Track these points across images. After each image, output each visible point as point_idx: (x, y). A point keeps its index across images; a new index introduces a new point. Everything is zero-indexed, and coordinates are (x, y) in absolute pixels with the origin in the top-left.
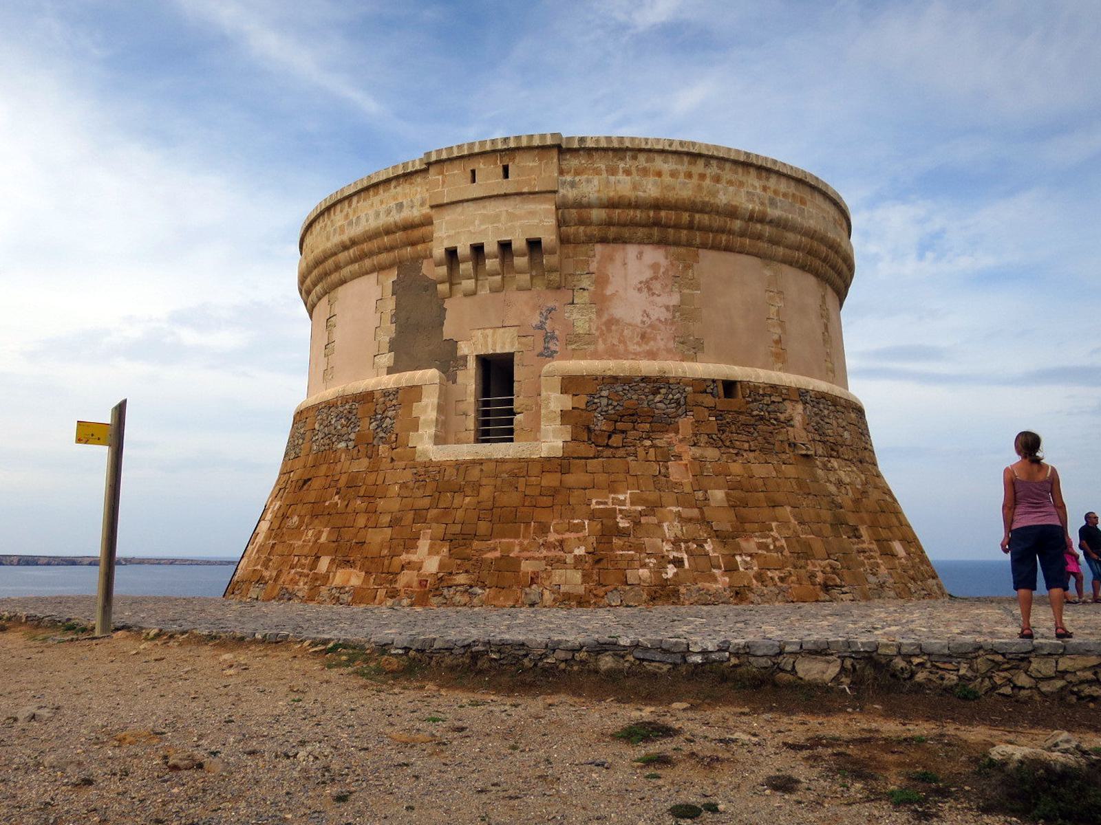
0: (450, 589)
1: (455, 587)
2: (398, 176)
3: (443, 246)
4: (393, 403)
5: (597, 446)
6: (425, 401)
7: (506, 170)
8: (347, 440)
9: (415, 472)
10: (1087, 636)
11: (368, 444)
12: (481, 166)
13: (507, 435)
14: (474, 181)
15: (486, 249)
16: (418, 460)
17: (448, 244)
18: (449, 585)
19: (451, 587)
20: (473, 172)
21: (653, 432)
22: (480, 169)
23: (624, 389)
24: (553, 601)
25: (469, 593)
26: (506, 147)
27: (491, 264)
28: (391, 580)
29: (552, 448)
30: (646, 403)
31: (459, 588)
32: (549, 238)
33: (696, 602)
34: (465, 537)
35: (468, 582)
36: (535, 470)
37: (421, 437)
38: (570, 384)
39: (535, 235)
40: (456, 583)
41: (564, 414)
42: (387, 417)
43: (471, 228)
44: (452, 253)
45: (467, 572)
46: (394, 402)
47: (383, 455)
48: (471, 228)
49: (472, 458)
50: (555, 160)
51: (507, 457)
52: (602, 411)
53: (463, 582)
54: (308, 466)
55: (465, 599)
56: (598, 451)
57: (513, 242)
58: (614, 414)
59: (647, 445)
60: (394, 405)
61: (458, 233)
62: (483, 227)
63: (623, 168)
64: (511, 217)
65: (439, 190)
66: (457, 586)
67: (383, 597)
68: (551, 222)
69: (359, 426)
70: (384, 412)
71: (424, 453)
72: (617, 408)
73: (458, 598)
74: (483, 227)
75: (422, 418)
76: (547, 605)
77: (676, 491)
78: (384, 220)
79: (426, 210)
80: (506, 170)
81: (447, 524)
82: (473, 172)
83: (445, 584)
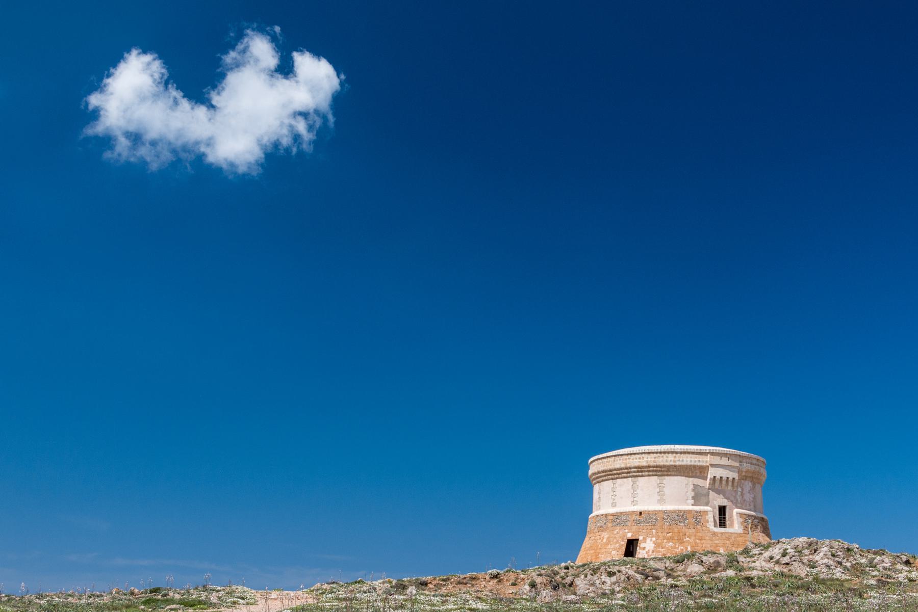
6: (709, 516)
71: (712, 529)
75: (709, 520)
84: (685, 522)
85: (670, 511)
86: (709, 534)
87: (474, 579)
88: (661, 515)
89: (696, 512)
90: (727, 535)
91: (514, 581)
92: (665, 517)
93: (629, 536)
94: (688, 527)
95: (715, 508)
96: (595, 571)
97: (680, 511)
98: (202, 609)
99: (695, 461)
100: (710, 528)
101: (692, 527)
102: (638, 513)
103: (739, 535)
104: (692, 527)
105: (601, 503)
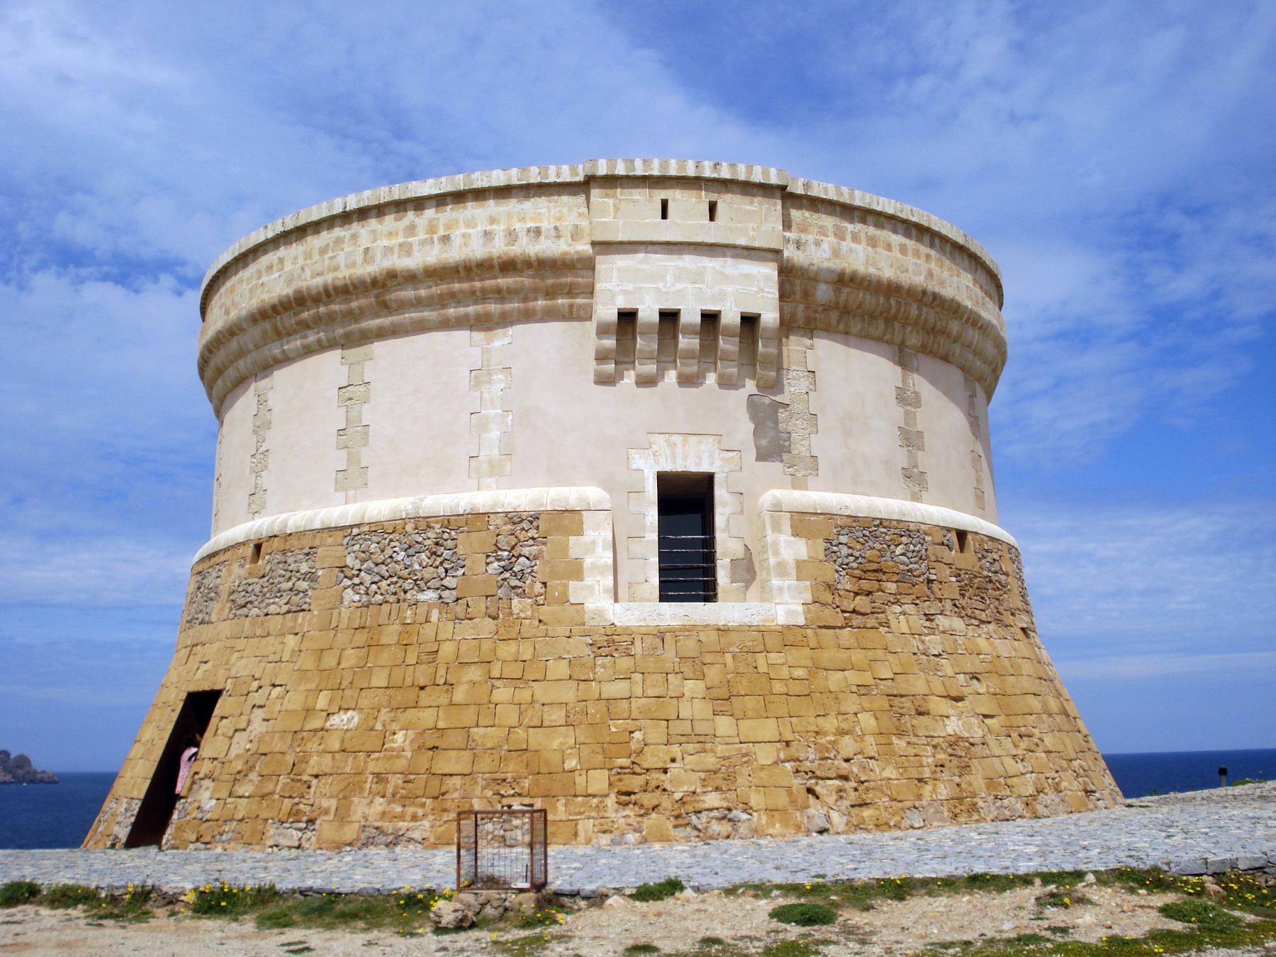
0: (699, 815)
1: (706, 812)
2: (528, 184)
3: (614, 304)
4: (530, 534)
5: (843, 611)
6: (590, 534)
7: (712, 208)
8: (437, 589)
9: (591, 642)
10: (849, 873)
11: (487, 597)
12: (676, 197)
13: (708, 592)
14: (664, 216)
15: (684, 319)
16: (592, 623)
17: (623, 303)
18: (697, 810)
19: (700, 812)
20: (665, 205)
21: (900, 594)
22: (674, 200)
23: (864, 535)
24: (847, 824)
25: (730, 820)
26: (716, 175)
27: (687, 342)
28: (597, 806)
29: (790, 613)
30: (888, 554)
31: (712, 814)
32: (770, 316)
33: (996, 818)
34: (701, 739)
35: (725, 804)
36: (772, 642)
37: (591, 589)
38: (803, 522)
39: (752, 309)
40: (706, 806)
41: (800, 564)
42: (520, 555)
43: (660, 285)
44: (627, 317)
45: (717, 789)
46: (532, 533)
47: (522, 615)
48: (660, 285)
49: (681, 623)
50: (779, 207)
51: (732, 624)
52: (842, 564)
53: (717, 804)
54: (343, 625)
55: (725, 828)
56: (845, 618)
57: (723, 314)
58: (857, 568)
59: (896, 611)
60: (533, 538)
61: (640, 288)
62: (679, 286)
63: (852, 232)
64: (406, 249)
65: (607, 220)
66: (711, 810)
67: (590, 833)
68: (772, 292)
69: (464, 566)
70: (513, 548)
71: (599, 613)
72: (860, 560)
73: (716, 827)
74: (679, 286)
75: (588, 561)
76: (840, 830)
77: (939, 673)
78: (499, 248)
79: (584, 248)
80: (712, 208)
81: (668, 721)
82: (665, 205)
83: (690, 809)
84: (449, 582)
85: (377, 529)
86: (579, 647)
87: (936, 780)
88: (328, 553)
89: (514, 519)
90: (690, 647)
91: (998, 938)
92: (350, 561)
93: (1218, 775)
94: (460, 609)
95: (641, 492)
96: (1261, 797)
97: (423, 523)
98: (914, 385)
99: (917, 254)
100: (590, 605)
101: (479, 605)
102: (249, 550)
103: (787, 638)
104: (479, 605)
105: (266, 480)
